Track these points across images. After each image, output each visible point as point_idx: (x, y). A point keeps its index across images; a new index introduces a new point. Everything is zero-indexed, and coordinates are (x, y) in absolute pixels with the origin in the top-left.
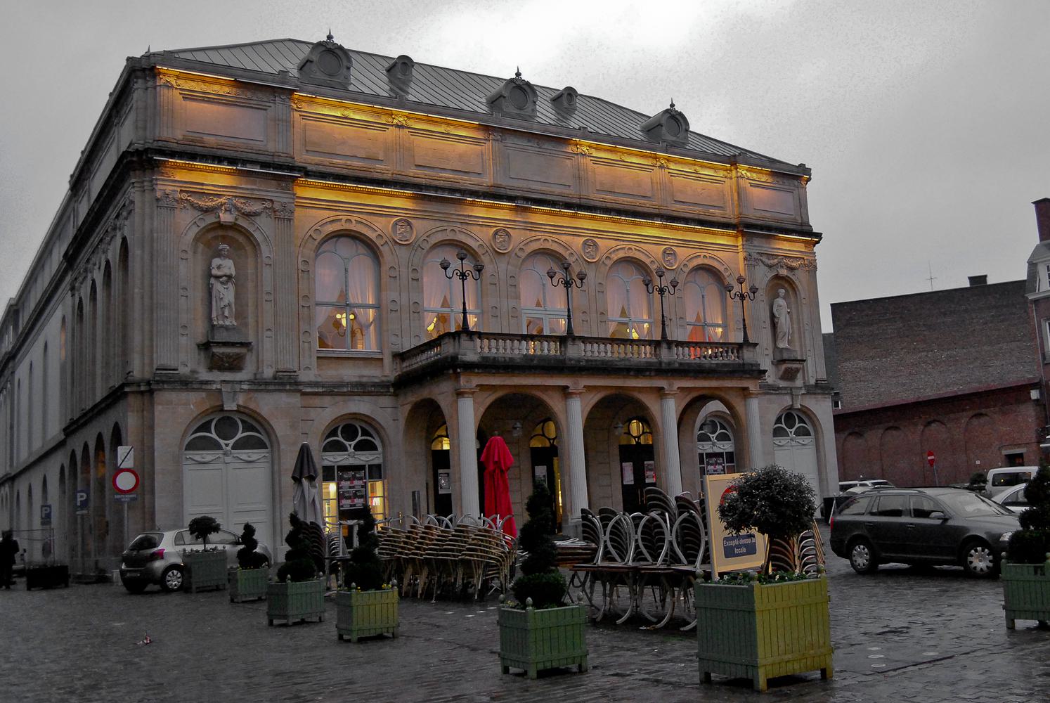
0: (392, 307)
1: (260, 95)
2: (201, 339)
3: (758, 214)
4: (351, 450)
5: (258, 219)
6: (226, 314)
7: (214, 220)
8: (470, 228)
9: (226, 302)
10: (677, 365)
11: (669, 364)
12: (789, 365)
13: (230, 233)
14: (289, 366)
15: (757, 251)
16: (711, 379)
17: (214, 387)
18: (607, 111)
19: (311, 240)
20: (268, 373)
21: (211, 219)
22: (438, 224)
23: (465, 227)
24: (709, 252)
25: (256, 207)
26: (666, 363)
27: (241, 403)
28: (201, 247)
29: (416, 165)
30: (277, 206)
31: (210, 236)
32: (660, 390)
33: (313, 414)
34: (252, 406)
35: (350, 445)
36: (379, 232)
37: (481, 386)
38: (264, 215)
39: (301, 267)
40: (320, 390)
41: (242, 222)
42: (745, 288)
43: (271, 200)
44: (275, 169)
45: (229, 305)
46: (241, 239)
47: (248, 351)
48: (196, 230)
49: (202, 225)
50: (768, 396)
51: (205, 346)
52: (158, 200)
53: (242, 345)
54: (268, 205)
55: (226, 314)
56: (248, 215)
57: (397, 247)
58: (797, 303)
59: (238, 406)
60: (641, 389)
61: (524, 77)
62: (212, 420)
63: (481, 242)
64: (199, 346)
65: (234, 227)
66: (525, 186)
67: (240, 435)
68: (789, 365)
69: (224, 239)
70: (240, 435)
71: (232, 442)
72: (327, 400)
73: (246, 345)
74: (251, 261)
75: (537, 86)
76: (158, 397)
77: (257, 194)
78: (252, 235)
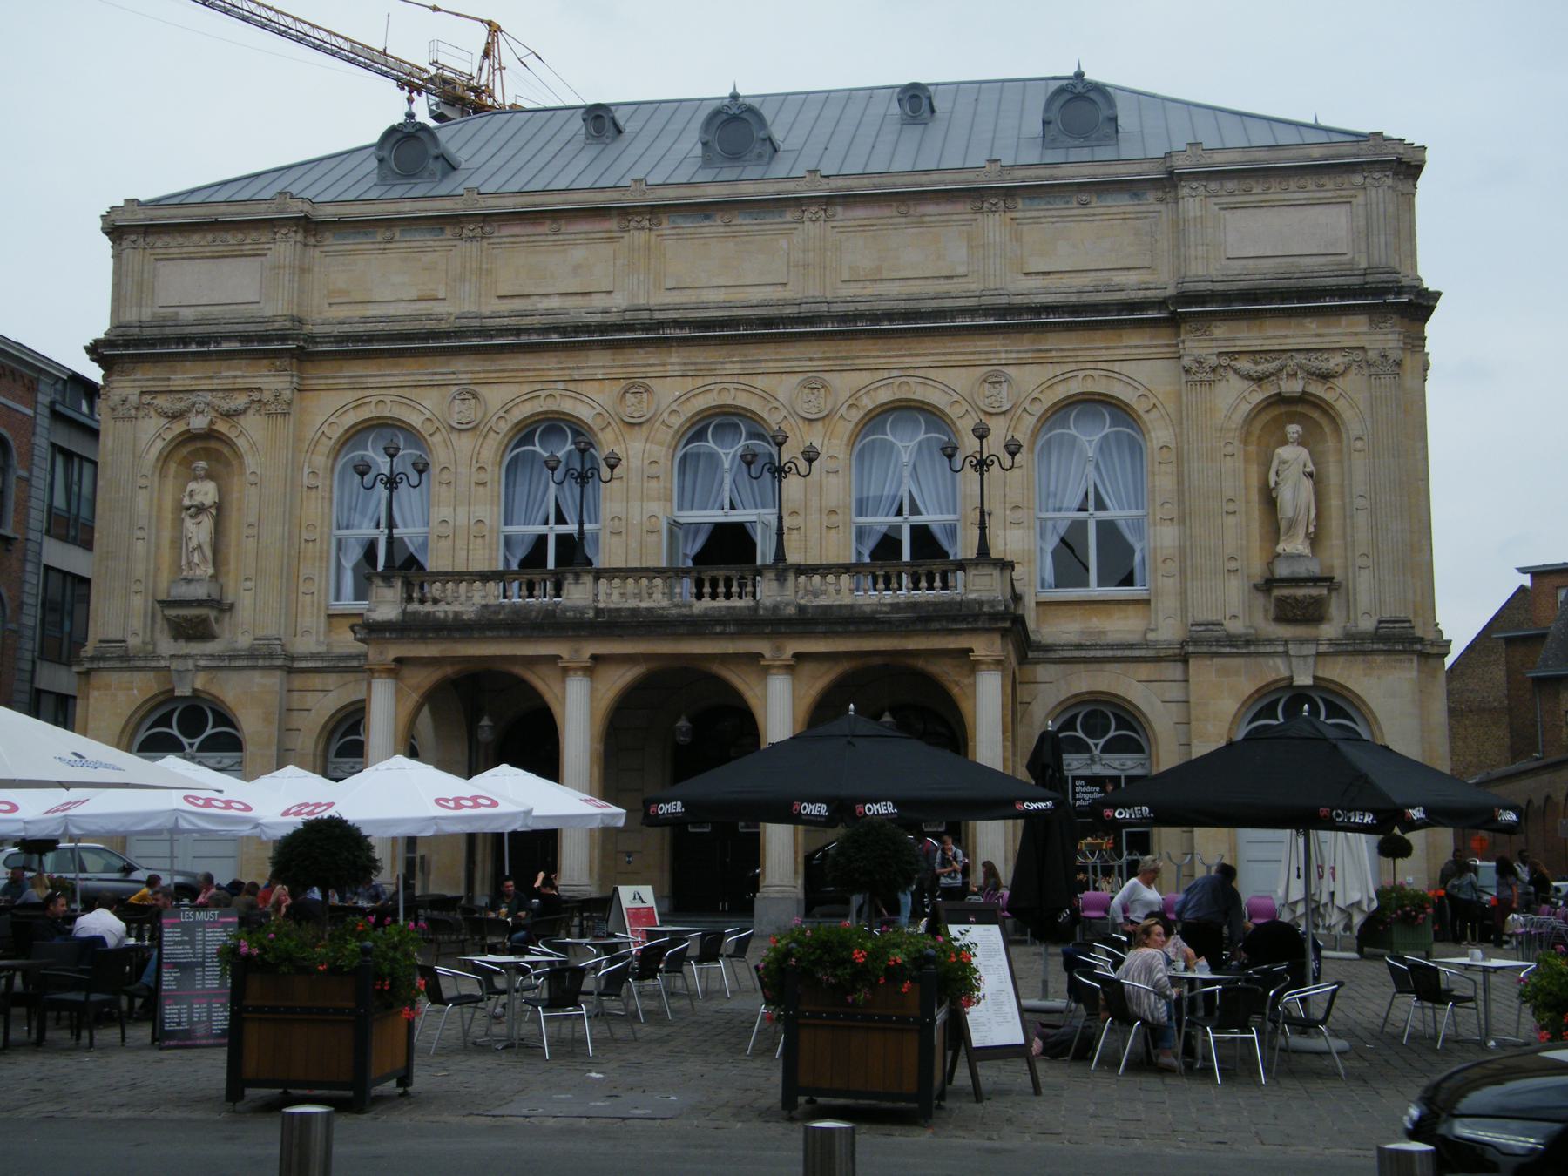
0: (443, 530)
1: (254, 235)
2: (1257, 569)
3: (1236, 267)
4: (1097, 752)
5: (242, 420)
6: (196, 560)
7: (184, 428)
8: (581, 387)
9: (193, 543)
10: (591, 614)
11: (776, 608)
12: (1286, 592)
13: (1299, 408)
14: (272, 631)
15: (1216, 351)
16: (483, 639)
17: (163, 663)
18: (492, 148)
19: (492, 434)
20: (1367, 624)
21: (179, 427)
22: (526, 388)
23: (571, 386)
24: (1100, 365)
25: (241, 401)
26: (766, 609)
27: (198, 686)
28: (172, 467)
29: (500, 297)
30: (267, 396)
31: (185, 451)
32: (756, 657)
33: (311, 700)
34: (214, 690)
35: (1096, 744)
36: (428, 415)
37: (799, 657)
38: (251, 412)
39: (306, 482)
40: (320, 664)
41: (1317, 389)
42: (994, 445)
43: (259, 389)
44: (1342, 298)
45: (200, 546)
46: (1316, 415)
47: (1330, 590)
48: (159, 444)
49: (169, 436)
50: (1217, 661)
51: (1269, 584)
52: (1187, 371)
53: (1315, 581)
54: (256, 396)
55: (196, 560)
56: (229, 415)
57: (454, 436)
58: (1340, 451)
59: (194, 690)
60: (724, 658)
61: (1090, 76)
62: (173, 711)
63: (599, 409)
64: (1256, 587)
65: (1304, 398)
66: (693, 299)
67: (209, 731)
68: (1286, 592)
69: (1292, 418)
70: (209, 731)
71: (197, 741)
72: (332, 680)
73: (1326, 581)
74: (1331, 443)
75: (1117, 88)
76: (97, 679)
77: (240, 383)
78: (1332, 407)
